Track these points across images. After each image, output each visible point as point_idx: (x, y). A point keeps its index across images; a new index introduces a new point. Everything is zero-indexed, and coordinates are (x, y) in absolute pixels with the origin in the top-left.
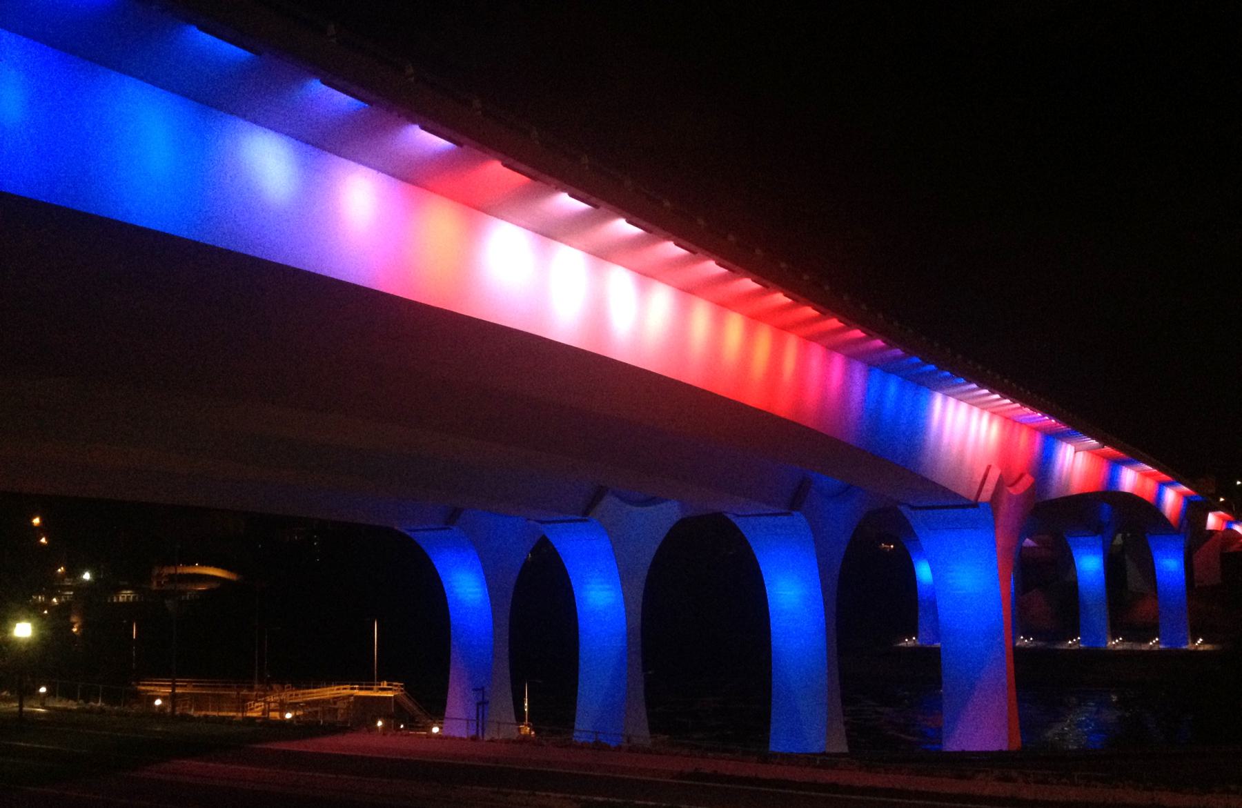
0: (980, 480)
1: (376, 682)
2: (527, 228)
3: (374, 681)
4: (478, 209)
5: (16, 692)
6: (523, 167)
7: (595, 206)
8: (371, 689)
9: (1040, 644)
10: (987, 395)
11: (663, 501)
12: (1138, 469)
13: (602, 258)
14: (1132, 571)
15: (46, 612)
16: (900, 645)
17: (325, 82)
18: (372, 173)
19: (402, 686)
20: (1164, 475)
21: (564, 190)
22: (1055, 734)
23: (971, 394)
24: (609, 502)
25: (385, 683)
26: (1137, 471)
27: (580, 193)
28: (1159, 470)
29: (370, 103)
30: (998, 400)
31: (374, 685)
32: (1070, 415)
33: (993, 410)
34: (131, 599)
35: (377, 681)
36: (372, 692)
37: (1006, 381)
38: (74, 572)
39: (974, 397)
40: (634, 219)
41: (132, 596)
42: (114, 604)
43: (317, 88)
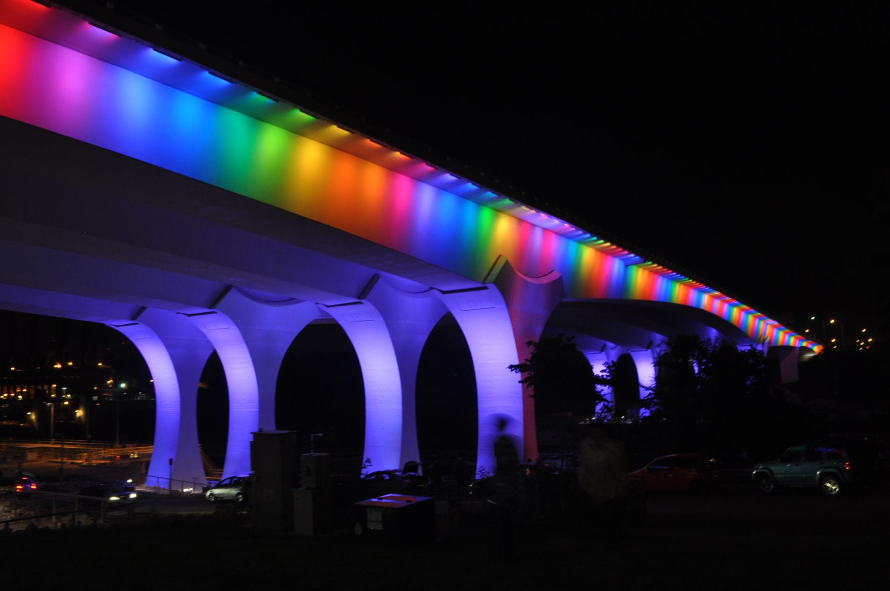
0: (486, 272)
2: (87, 54)
4: (46, 39)
5: (613, 413)
6: (311, 112)
7: (480, 187)
10: (602, 243)
11: (300, 301)
13: (169, 85)
14: (225, 483)
15: (95, 388)
17: (155, 50)
18: (407, 178)
21: (448, 173)
23: (669, 275)
24: (232, 296)
27: (375, 140)
28: (664, 267)
29: (277, 101)
30: (602, 243)
40: (341, 125)
41: (145, 397)
43: (206, 75)
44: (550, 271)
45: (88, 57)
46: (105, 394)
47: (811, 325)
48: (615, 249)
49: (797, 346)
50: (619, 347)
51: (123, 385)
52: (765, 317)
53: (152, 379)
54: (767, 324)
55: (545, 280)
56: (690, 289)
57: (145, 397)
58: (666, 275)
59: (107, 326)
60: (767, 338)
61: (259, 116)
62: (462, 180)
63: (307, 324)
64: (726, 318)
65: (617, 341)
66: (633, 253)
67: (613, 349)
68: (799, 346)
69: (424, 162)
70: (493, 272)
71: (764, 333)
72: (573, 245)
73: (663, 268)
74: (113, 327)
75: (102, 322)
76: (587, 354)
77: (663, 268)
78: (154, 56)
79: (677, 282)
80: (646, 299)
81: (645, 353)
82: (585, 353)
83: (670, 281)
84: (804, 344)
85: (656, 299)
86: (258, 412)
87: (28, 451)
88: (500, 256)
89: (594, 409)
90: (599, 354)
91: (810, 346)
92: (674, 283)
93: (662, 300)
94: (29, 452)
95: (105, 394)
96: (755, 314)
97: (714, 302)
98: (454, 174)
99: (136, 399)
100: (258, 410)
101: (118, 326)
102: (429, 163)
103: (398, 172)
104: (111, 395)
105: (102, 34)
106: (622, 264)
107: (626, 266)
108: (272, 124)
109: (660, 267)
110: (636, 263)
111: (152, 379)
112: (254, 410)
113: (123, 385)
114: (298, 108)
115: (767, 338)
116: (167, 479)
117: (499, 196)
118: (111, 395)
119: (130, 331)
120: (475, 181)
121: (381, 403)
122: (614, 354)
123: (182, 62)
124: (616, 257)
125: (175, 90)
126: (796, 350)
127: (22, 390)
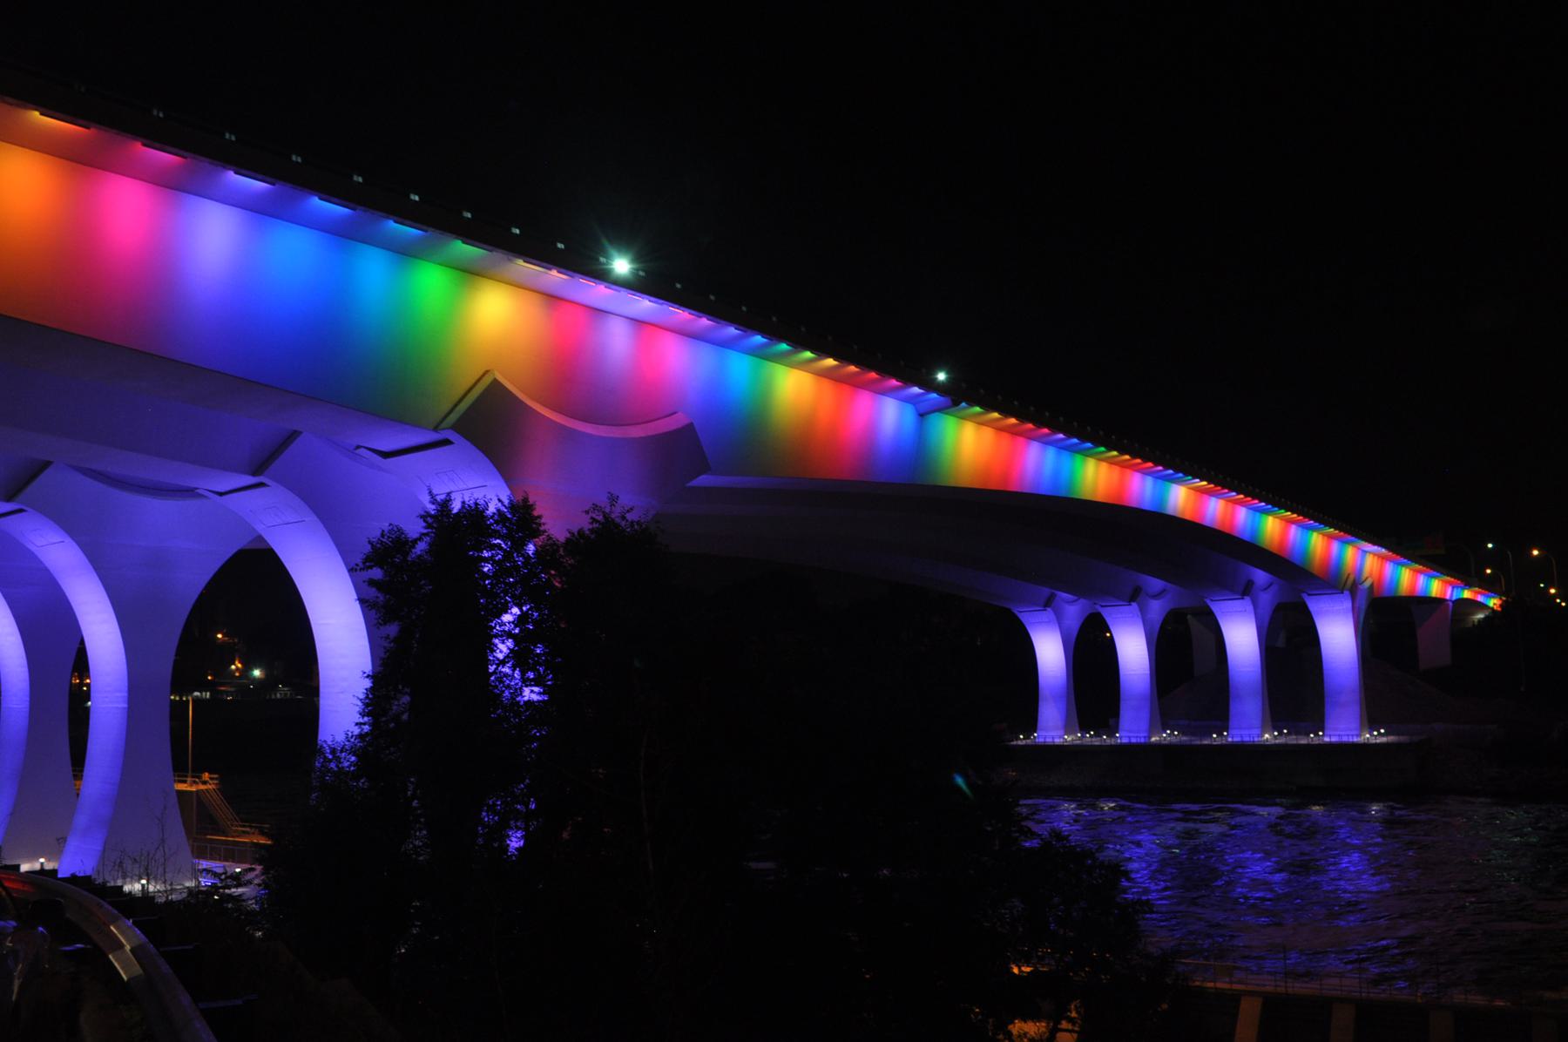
1: (190, 774)
3: (188, 772)
8: (185, 782)
9: (1185, 738)
12: (1411, 567)
16: (1012, 743)
19: (216, 779)
20: (1417, 565)
22: (205, 783)
25: (207, 774)
26: (1190, 488)
31: (186, 776)
32: (1271, 496)
33: (1156, 475)
34: (288, 695)
35: (193, 771)
36: (186, 785)
37: (1264, 493)
38: (248, 667)
39: (1109, 458)
41: (289, 693)
42: (274, 700)
44: (670, 412)
45: (57, 159)
46: (223, 688)
47: (1490, 559)
49: (1448, 597)
50: (1082, 601)
51: (257, 673)
53: (89, 677)
55: (636, 432)
57: (289, 693)
60: (1367, 578)
63: (239, 548)
64: (1246, 536)
66: (1115, 450)
67: (1265, 589)
68: (1454, 598)
69: (731, 326)
71: (1359, 571)
72: (864, 399)
78: (318, 204)
80: (993, 485)
84: (1466, 594)
85: (1027, 488)
88: (487, 372)
90: (1241, 601)
91: (1481, 599)
93: (1045, 488)
95: (223, 688)
99: (273, 697)
102: (325, 196)
103: (728, 347)
104: (233, 689)
105: (163, 158)
106: (909, 413)
107: (922, 415)
110: (940, 409)
111: (89, 677)
113: (257, 673)
115: (1367, 578)
116: (1452, 591)
118: (233, 689)
120: (763, 333)
122: (1075, 611)
123: (277, 185)
125: (202, 199)
126: (1448, 605)
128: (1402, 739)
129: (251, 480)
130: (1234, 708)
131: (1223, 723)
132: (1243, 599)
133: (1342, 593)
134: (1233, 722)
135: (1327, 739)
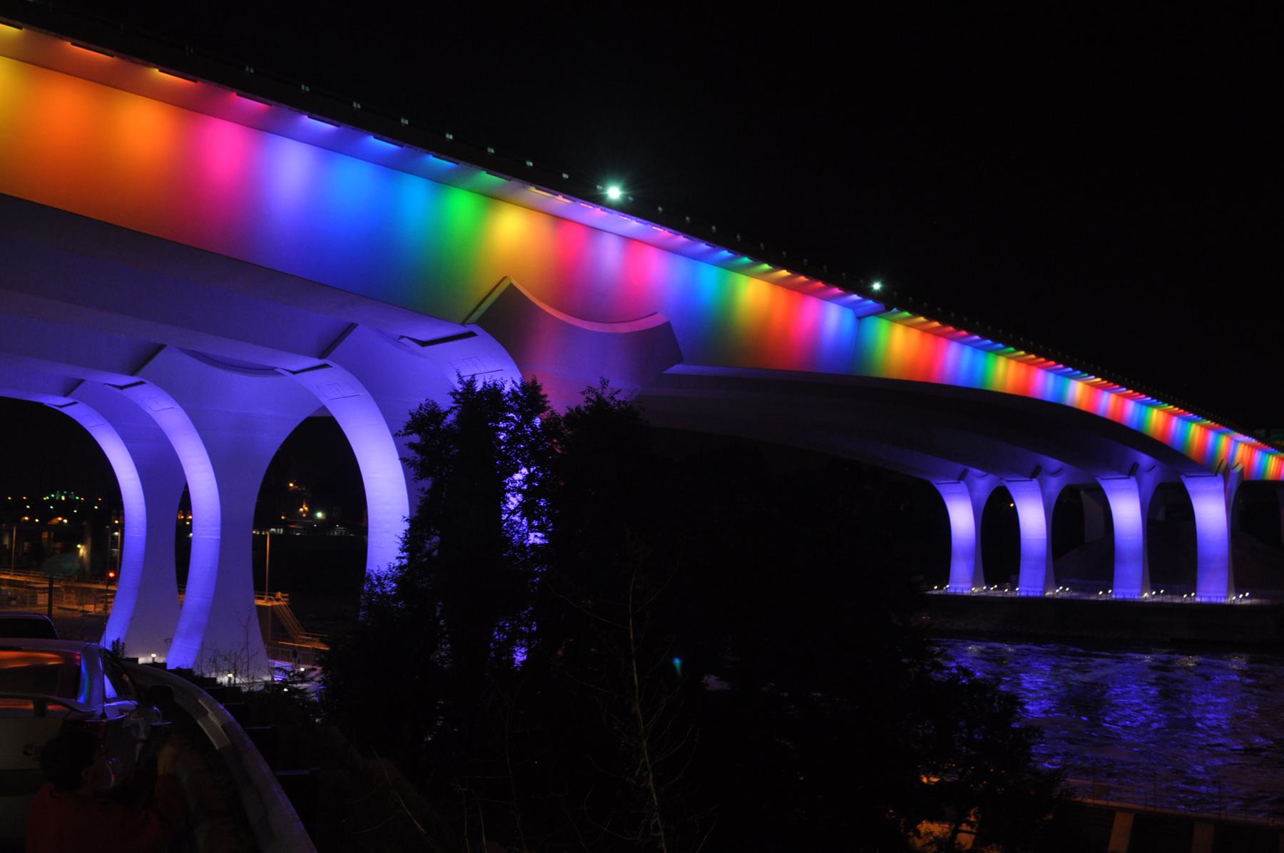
30: (1053, 365)
46: (293, 526)
48: (1033, 359)
51: (319, 515)
52: (1230, 431)
54: (1237, 442)
56: (1034, 369)
58: (1050, 368)
59: (46, 406)
60: (1238, 464)
61: (441, 180)
62: (460, 165)
65: (988, 466)
66: (1022, 350)
69: (483, 170)
70: (488, 300)
73: (1103, 380)
74: (51, 406)
75: (39, 401)
76: (938, 484)
77: (1103, 380)
78: (375, 143)
79: (1079, 381)
81: (1029, 483)
82: (933, 483)
83: (1185, 422)
86: (219, 541)
87: (38, 591)
89: (270, 528)
92: (1189, 423)
93: (962, 382)
94: (41, 593)
95: (293, 526)
96: (1201, 423)
97: (1171, 420)
98: (314, 115)
99: (332, 534)
100: (219, 537)
101: (61, 407)
104: (300, 527)
106: (849, 316)
107: (860, 318)
108: (460, 188)
109: (1105, 382)
110: (876, 313)
112: (216, 537)
114: (533, 186)
115: (1238, 464)
117: (775, 268)
118: (300, 527)
119: (81, 413)
120: (730, 249)
121: (386, 532)
122: (984, 485)
123: (341, 127)
124: (1133, 400)
127: (1244, 595)
128: (1265, 602)
129: (317, 362)
130: (1119, 570)
131: (1107, 579)
132: (1129, 478)
133: (1216, 476)
134: (1116, 582)
135: (1198, 600)
